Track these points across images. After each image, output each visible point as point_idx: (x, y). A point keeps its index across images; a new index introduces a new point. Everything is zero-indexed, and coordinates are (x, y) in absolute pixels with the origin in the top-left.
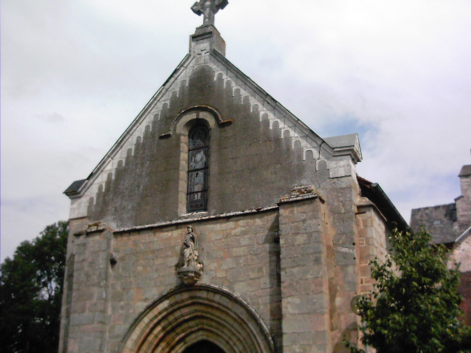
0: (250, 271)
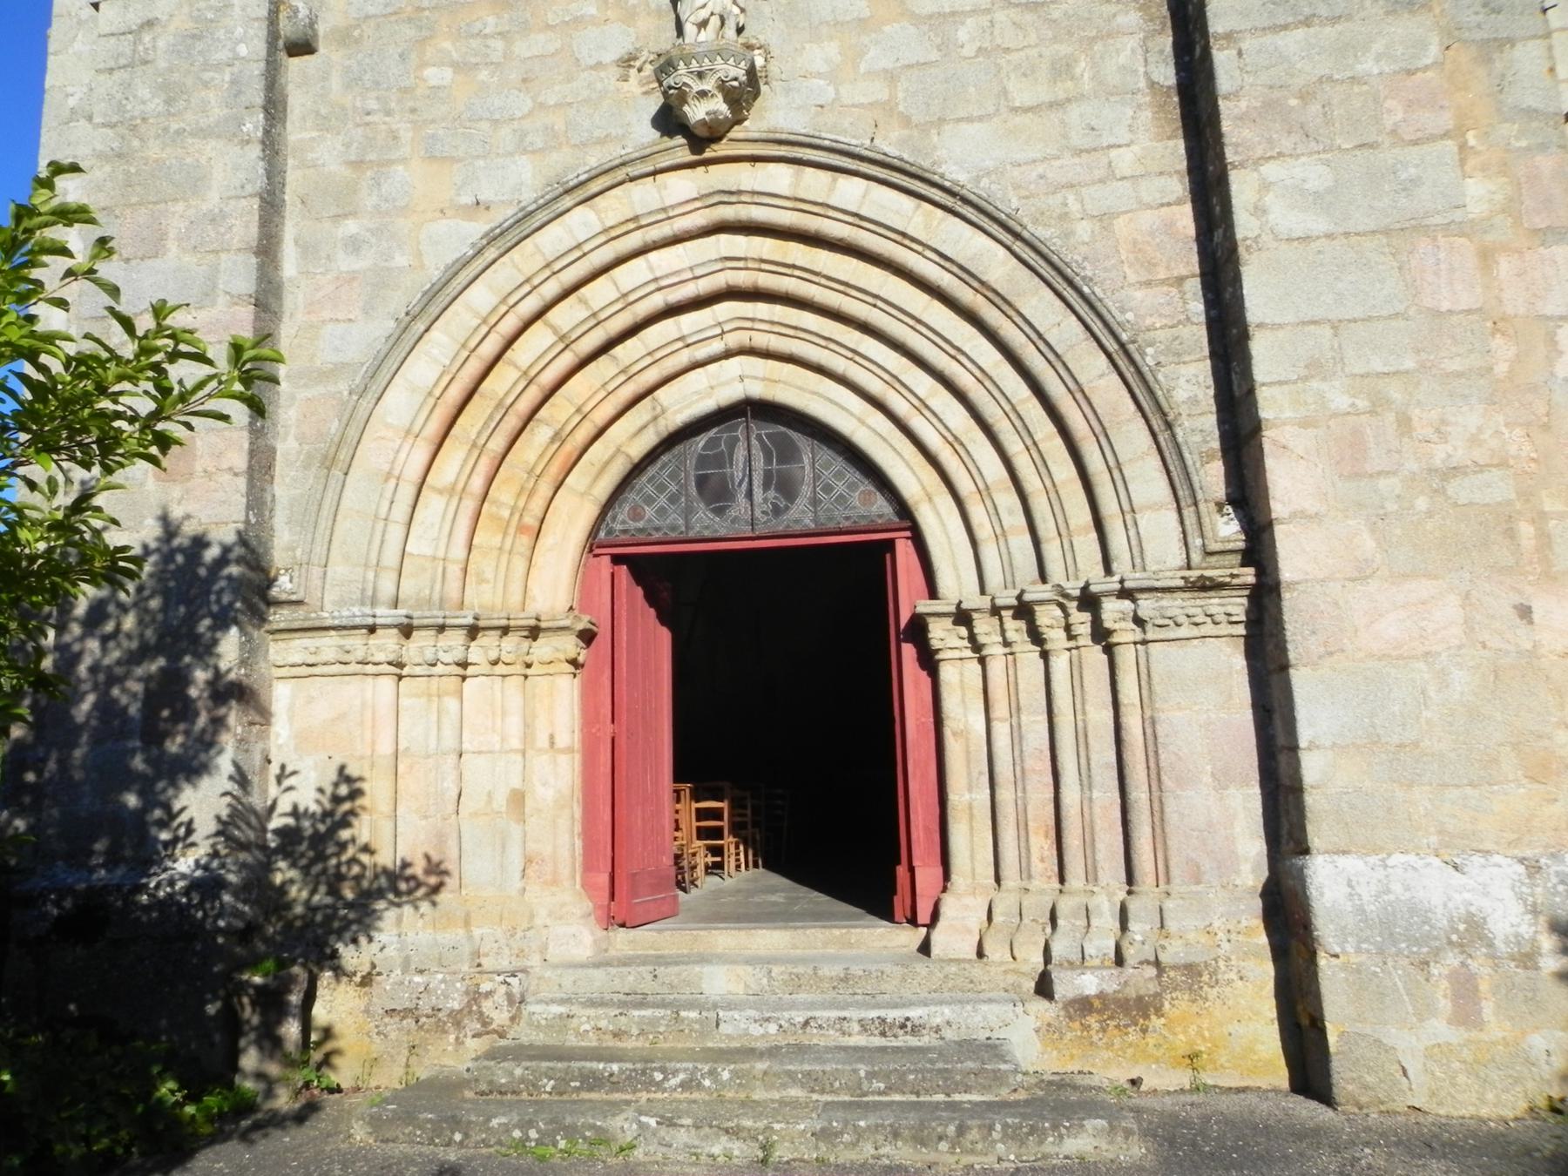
0: (1013, 76)
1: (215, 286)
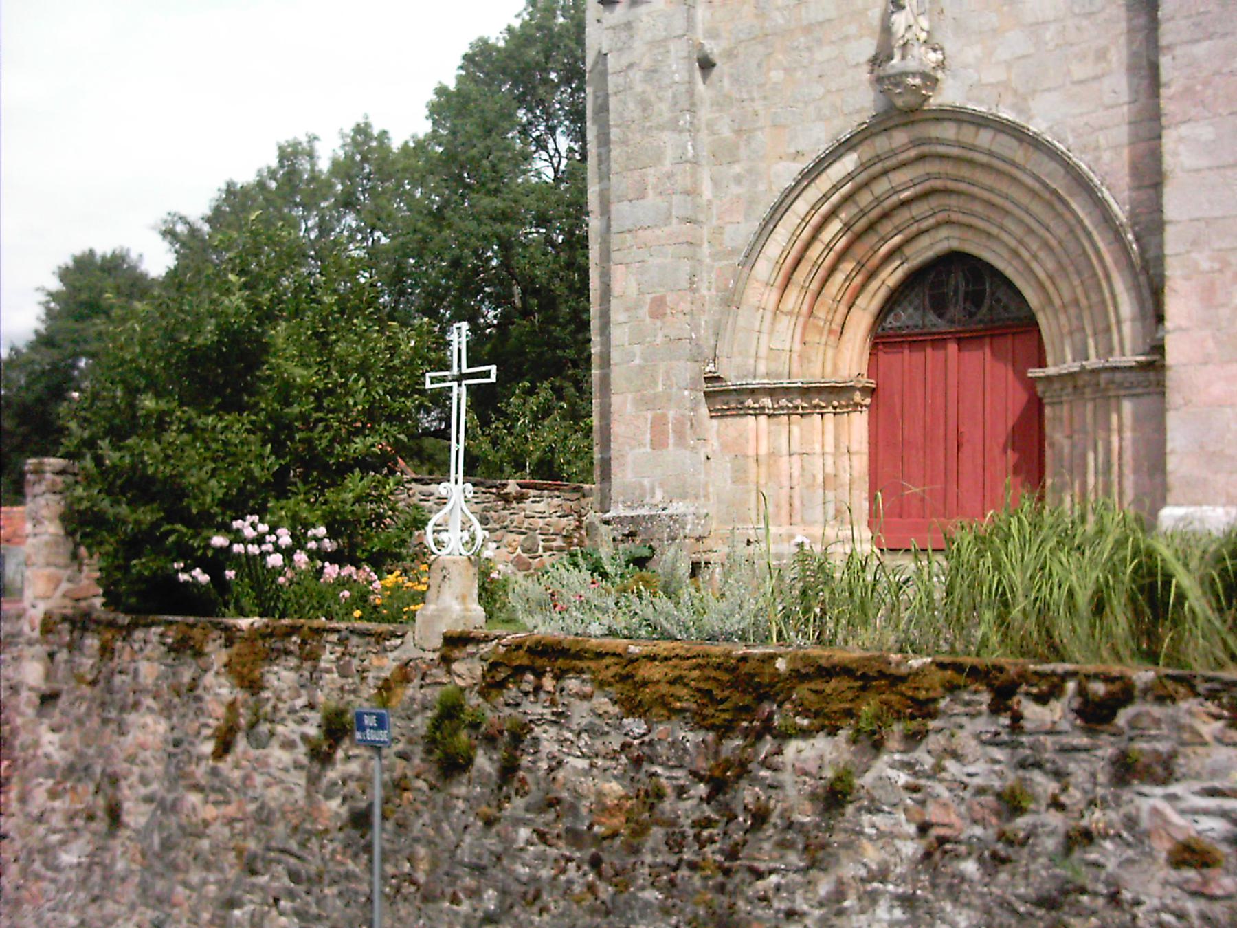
1: (671, 214)
